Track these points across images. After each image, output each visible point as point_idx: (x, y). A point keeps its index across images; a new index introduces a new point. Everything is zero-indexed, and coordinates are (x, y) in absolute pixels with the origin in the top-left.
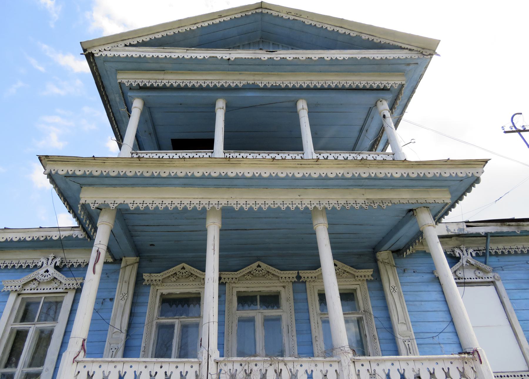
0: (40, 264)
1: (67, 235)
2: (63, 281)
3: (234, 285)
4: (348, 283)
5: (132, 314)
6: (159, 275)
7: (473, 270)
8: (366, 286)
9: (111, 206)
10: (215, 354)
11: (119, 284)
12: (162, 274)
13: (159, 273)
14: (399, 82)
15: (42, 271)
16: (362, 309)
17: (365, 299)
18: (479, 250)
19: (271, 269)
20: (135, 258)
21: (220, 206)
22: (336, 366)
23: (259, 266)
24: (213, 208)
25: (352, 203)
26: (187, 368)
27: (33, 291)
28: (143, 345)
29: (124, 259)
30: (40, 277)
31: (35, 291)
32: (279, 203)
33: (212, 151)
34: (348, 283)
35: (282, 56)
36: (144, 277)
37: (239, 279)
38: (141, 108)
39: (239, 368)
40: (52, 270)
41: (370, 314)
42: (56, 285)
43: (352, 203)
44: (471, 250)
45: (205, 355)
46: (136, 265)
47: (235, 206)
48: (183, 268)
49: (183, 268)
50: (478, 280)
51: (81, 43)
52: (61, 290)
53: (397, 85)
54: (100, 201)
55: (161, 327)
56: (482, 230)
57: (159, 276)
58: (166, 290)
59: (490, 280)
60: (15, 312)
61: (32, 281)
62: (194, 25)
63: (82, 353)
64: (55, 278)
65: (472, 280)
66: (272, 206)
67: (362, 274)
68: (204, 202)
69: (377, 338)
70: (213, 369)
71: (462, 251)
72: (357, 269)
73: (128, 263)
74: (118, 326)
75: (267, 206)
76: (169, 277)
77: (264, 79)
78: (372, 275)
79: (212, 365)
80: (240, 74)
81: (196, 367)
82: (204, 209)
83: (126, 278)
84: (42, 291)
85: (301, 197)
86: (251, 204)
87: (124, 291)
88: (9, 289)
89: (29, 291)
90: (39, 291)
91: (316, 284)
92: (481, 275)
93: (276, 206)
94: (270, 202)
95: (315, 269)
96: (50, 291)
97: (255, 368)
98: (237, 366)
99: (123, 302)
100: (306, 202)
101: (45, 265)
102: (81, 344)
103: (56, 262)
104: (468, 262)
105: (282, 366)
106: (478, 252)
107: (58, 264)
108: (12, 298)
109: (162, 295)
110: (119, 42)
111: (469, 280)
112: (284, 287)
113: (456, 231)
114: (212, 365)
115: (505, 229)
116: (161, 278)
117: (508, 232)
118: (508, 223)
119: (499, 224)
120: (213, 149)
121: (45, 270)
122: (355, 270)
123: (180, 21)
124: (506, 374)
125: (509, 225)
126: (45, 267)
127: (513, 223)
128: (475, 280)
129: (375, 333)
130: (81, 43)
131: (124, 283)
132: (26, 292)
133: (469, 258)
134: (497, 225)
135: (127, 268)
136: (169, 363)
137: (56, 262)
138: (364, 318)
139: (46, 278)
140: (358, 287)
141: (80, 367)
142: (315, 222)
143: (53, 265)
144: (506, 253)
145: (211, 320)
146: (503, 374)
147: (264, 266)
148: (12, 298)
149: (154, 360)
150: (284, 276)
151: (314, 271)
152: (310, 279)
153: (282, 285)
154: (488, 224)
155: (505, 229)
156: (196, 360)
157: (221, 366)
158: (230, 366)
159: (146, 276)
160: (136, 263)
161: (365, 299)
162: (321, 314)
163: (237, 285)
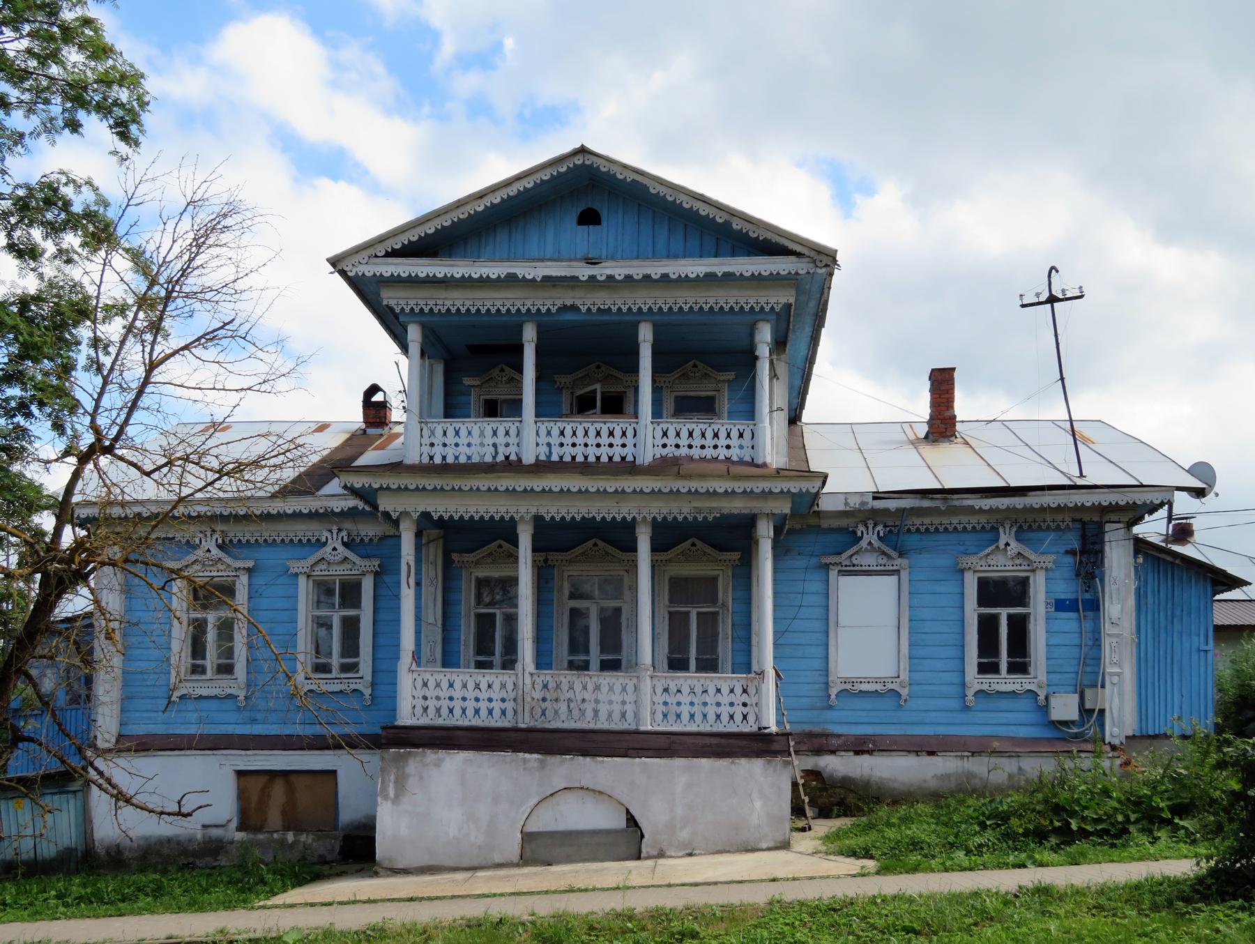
0: (324, 539)
1: (351, 506)
2: (357, 562)
3: (564, 568)
4: (709, 568)
5: (445, 603)
6: (471, 555)
8: (730, 574)
9: (413, 514)
11: (423, 566)
12: (475, 554)
15: (328, 549)
16: (720, 601)
17: (725, 591)
18: (895, 526)
19: (610, 549)
20: (437, 531)
21: (530, 515)
23: (595, 545)
24: (522, 517)
25: (675, 512)
28: (463, 638)
29: (424, 532)
30: (328, 557)
31: (327, 573)
32: (594, 513)
33: (520, 419)
34: (709, 568)
35: (609, 272)
36: (453, 557)
38: (420, 340)
39: (551, 680)
40: (341, 549)
41: (728, 609)
43: (675, 512)
44: (880, 528)
46: (441, 541)
47: (545, 515)
49: (500, 546)
52: (356, 572)
53: (780, 306)
54: (400, 509)
55: (479, 617)
56: (892, 504)
58: (482, 573)
60: (310, 596)
61: (320, 560)
62: (479, 200)
63: (414, 664)
64: (346, 558)
65: (871, 568)
66: (586, 516)
67: (725, 558)
68: (512, 510)
69: (730, 637)
70: (528, 681)
71: (867, 528)
72: (720, 551)
73: (432, 538)
74: (431, 620)
75: (581, 515)
76: (484, 557)
77: (589, 296)
78: (739, 560)
79: (527, 676)
80: (554, 286)
81: (513, 678)
82: (512, 518)
83: (431, 558)
84: (334, 573)
85: (619, 505)
86: (563, 513)
87: (432, 574)
88: (296, 570)
90: (331, 573)
91: (668, 568)
92: (885, 561)
93: (591, 516)
94: (584, 512)
95: (667, 551)
96: (344, 573)
97: (564, 680)
98: (548, 678)
99: (432, 589)
101: (330, 541)
102: (411, 656)
103: (343, 537)
104: (870, 543)
105: (587, 679)
106: (893, 529)
107: (345, 539)
108: (302, 581)
109: (477, 577)
110: (376, 246)
111: (867, 568)
112: (627, 571)
113: (857, 506)
114: (527, 676)
115: (926, 503)
116: (474, 559)
117: (929, 508)
118: (931, 496)
119: (919, 496)
120: (521, 416)
121: (332, 547)
122: (717, 552)
123: (459, 201)
124: (866, 680)
125: (932, 499)
126: (330, 544)
127: (938, 496)
128: (875, 568)
130: (335, 262)
131: (430, 565)
134: (916, 498)
135: (431, 545)
136: (490, 673)
137: (343, 537)
138: (721, 613)
139: (336, 558)
140: (721, 572)
141: (415, 675)
142: (638, 530)
143: (340, 540)
145: (525, 637)
146: (863, 680)
147: (601, 544)
149: (477, 671)
150: (626, 558)
151: (665, 553)
152: (659, 563)
153: (627, 568)
154: (904, 496)
155: (926, 503)
156: (512, 672)
157: (535, 677)
158: (542, 678)
159: (455, 556)
160: (440, 538)
161: (725, 591)
162: (670, 607)
163: (568, 568)
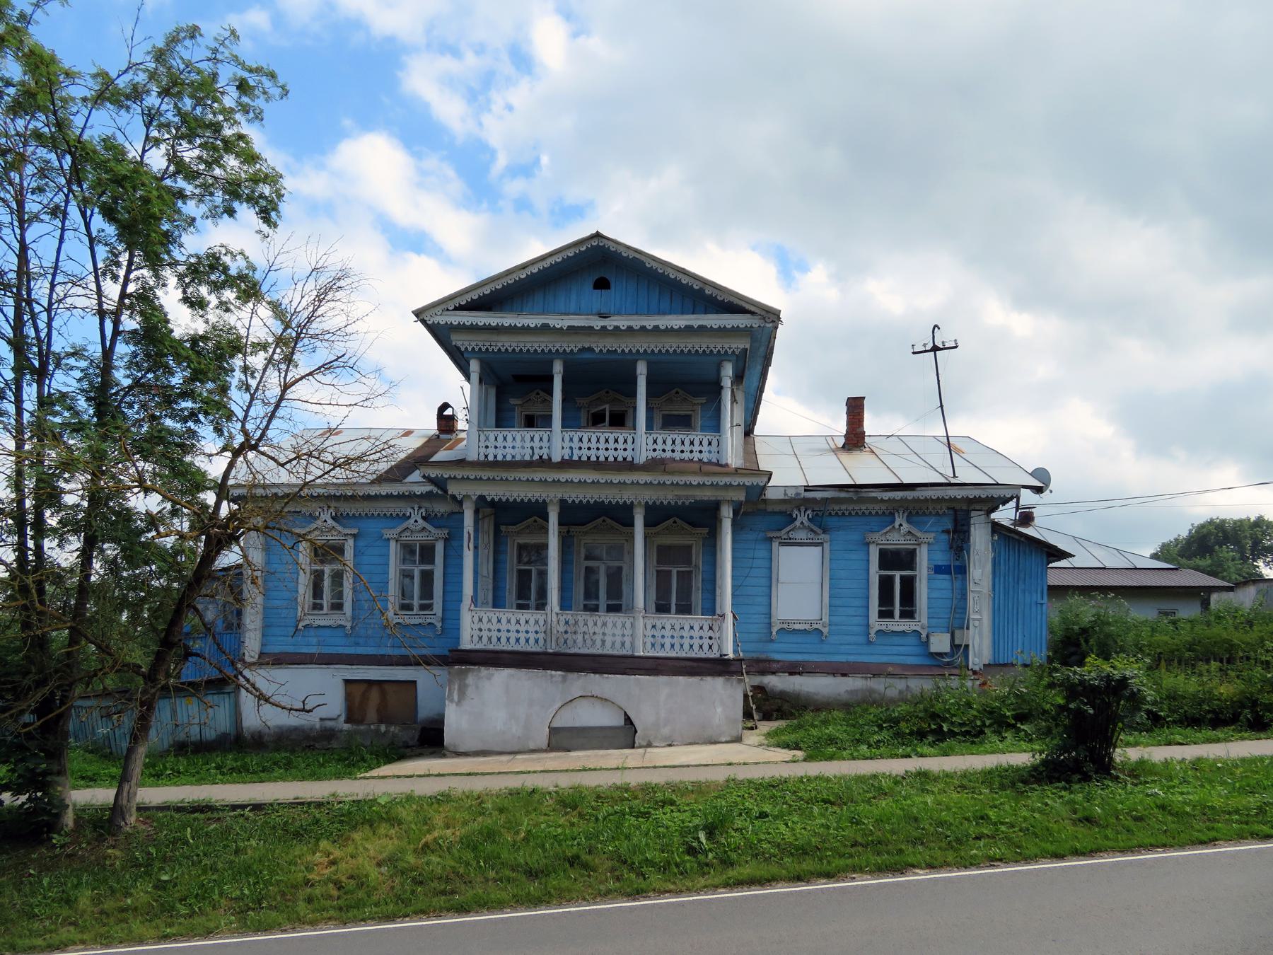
0: (408, 514)
2: (432, 531)
5: (496, 562)
7: (805, 531)
10: (556, 609)
13: (514, 525)
14: (741, 346)
15: (412, 521)
22: (631, 620)
26: (539, 616)
27: (408, 538)
28: (508, 587)
31: (410, 538)
35: (616, 324)
37: (586, 533)
38: (479, 371)
42: (427, 534)
45: (549, 608)
46: (493, 517)
48: (535, 521)
50: (808, 541)
51: (418, 313)
55: (520, 571)
57: (511, 528)
59: (820, 541)
62: (522, 271)
65: (803, 541)
70: (554, 619)
74: (485, 573)
79: (554, 615)
81: (544, 616)
89: (405, 538)
90: (413, 538)
98: (569, 617)
100: (625, 498)
101: (412, 515)
104: (802, 523)
108: (393, 544)
111: (800, 541)
112: (627, 540)
114: (554, 615)
115: (843, 495)
128: (806, 541)
129: (700, 585)
130: (418, 313)
132: (402, 538)
133: (805, 520)
141: (473, 613)
144: (847, 514)
147: (609, 521)
148: (393, 544)
155: (843, 495)
158: (565, 616)
159: (503, 528)
